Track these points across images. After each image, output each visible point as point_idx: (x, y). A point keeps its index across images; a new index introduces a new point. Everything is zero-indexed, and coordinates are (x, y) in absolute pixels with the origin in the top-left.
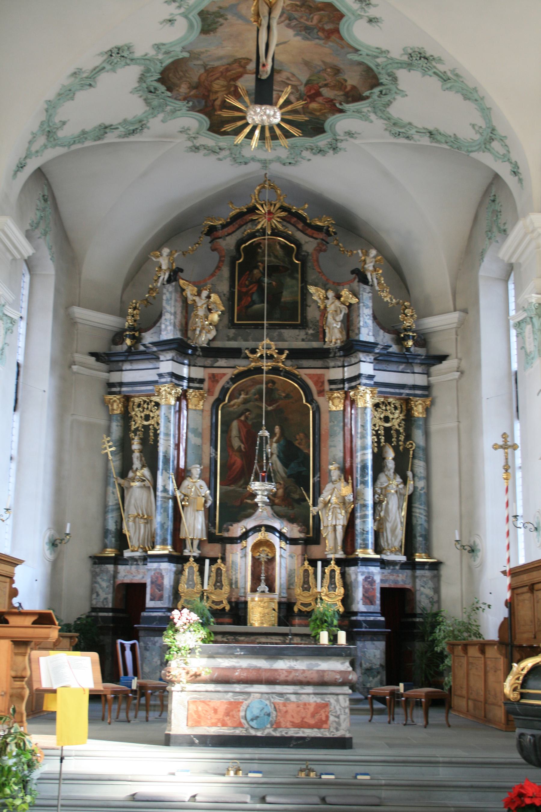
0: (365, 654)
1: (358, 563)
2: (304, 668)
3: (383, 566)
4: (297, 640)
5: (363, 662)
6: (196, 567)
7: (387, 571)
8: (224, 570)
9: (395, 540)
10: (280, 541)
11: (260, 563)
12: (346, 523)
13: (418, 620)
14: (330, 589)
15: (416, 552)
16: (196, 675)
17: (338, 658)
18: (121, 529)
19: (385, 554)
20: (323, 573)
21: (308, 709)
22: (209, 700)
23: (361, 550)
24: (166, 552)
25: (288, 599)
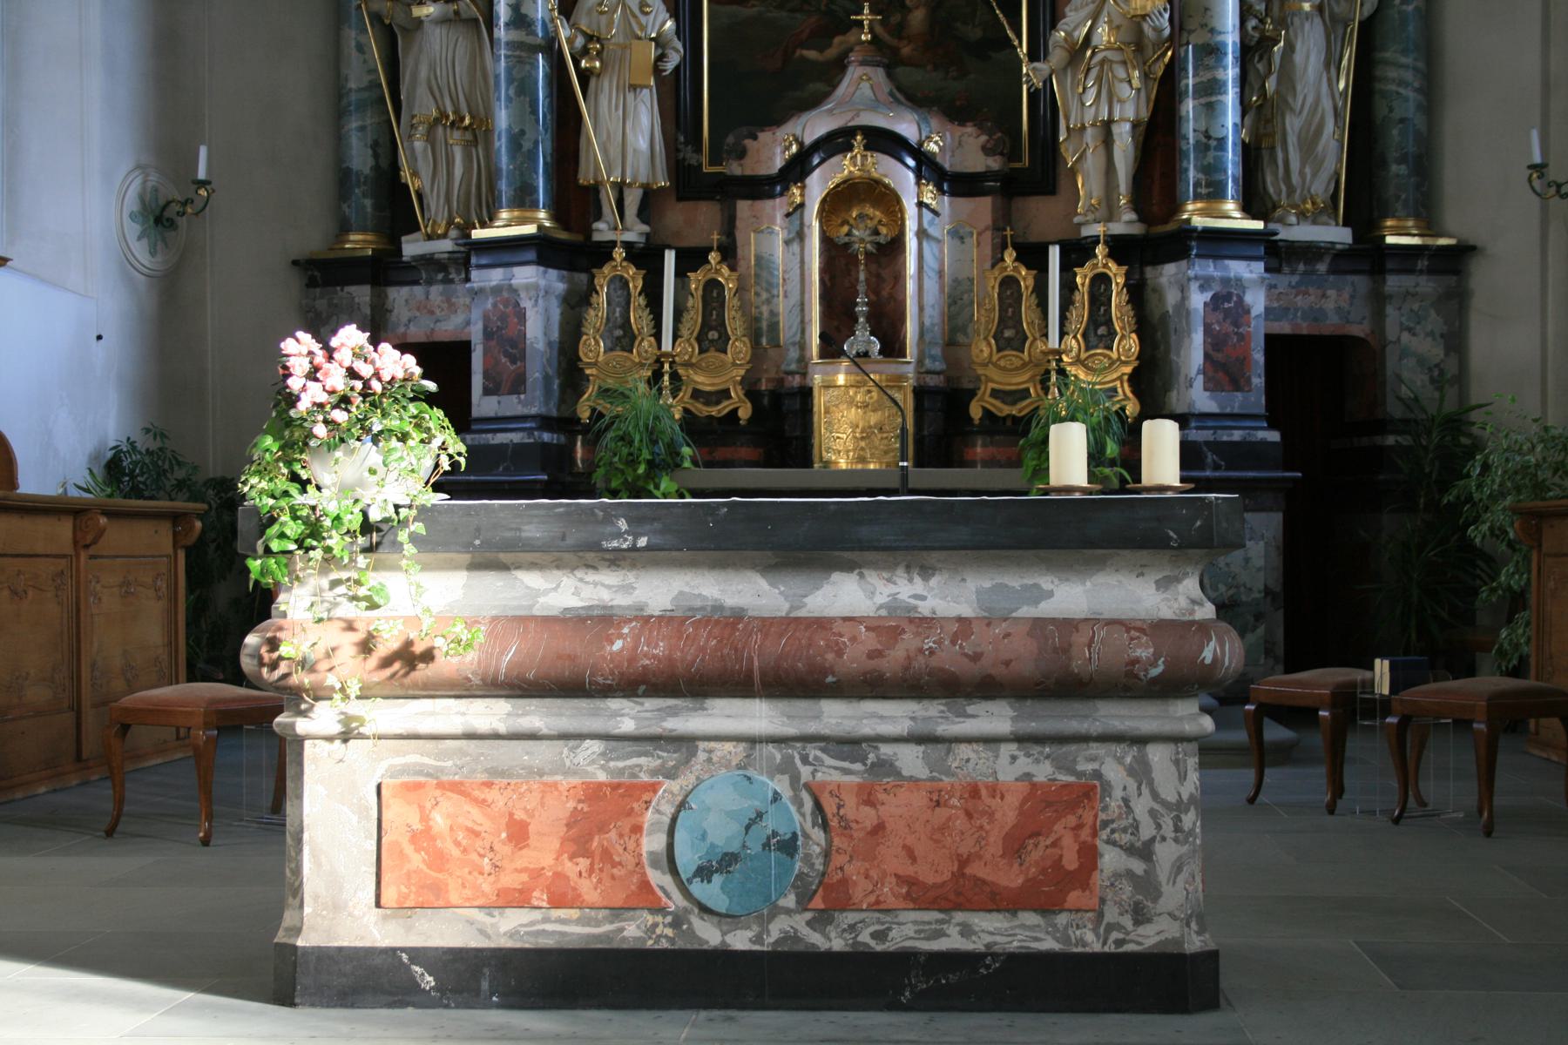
1: (1189, 249)
2: (967, 611)
3: (1274, 263)
6: (635, 279)
7: (1284, 281)
9: (1314, 175)
10: (918, 183)
11: (854, 259)
12: (1145, 115)
13: (1391, 440)
14: (1093, 339)
15: (1386, 216)
16: (409, 657)
17: (1144, 555)
18: (395, 167)
19: (1281, 220)
20: (1068, 287)
22: (483, 777)
23: (1199, 205)
24: (530, 229)
25: (948, 379)
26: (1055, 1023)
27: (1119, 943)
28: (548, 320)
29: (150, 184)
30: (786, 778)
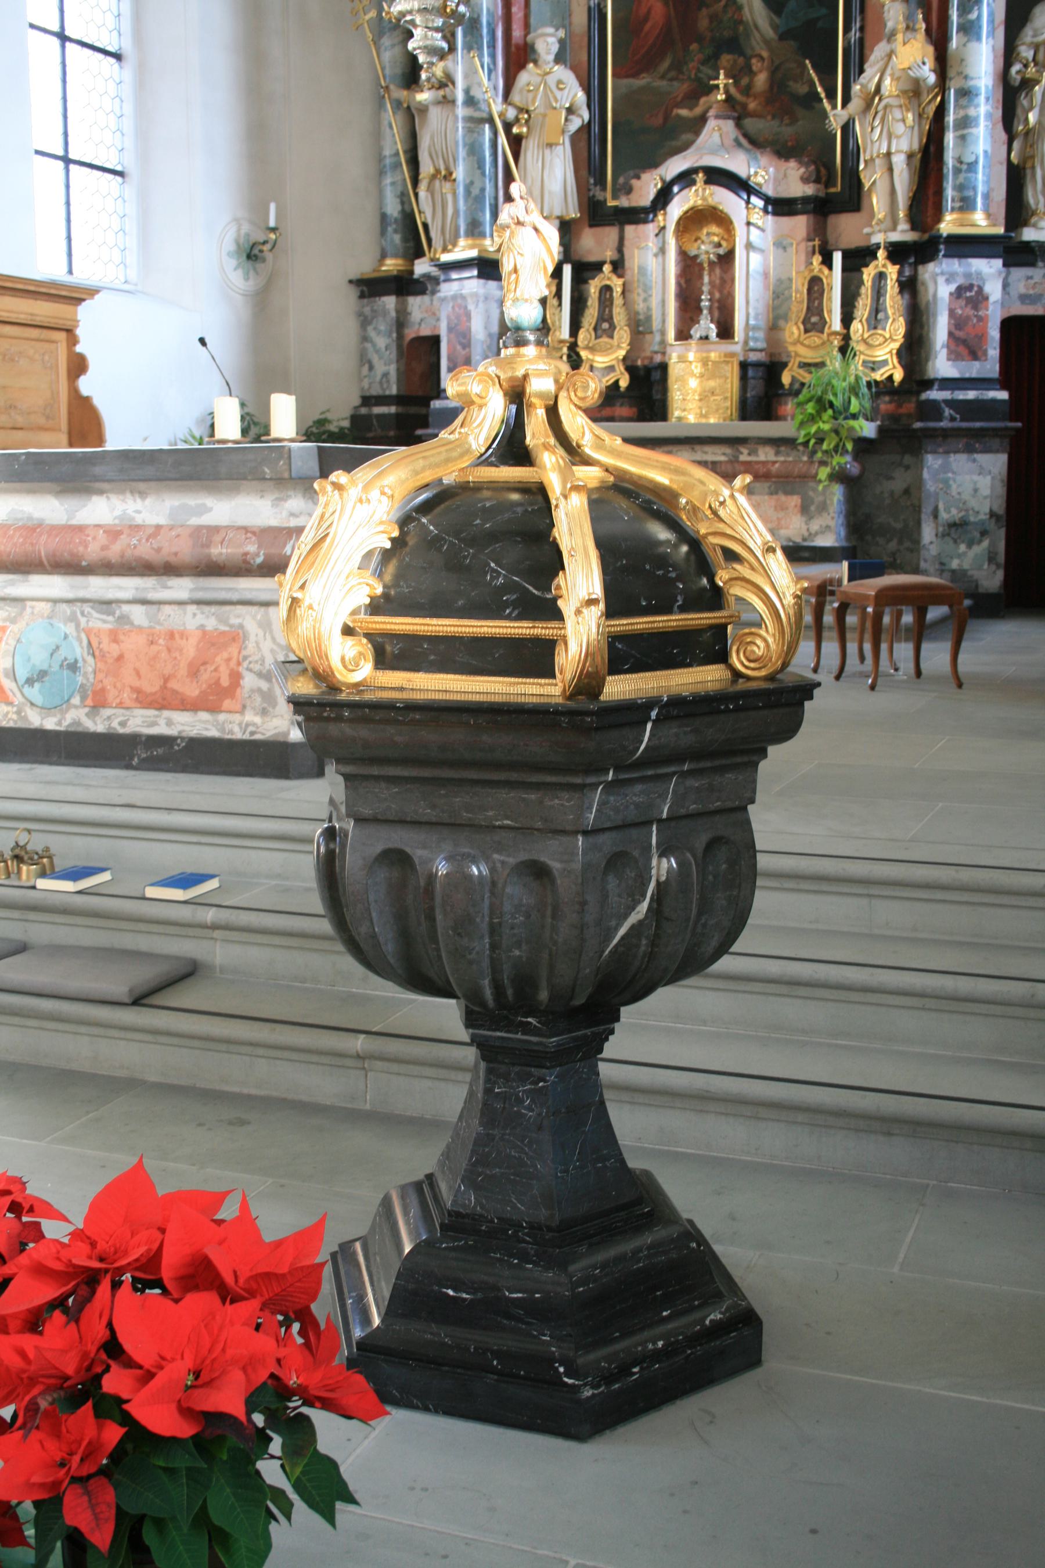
0: (949, 487)
2: (162, 521)
4: (766, 454)
5: (941, 506)
8: (618, 290)
11: (701, 265)
21: (181, 650)
25: (771, 355)
26: (168, 781)
27: (252, 733)
28: (488, 317)
29: (243, 232)
30: (73, 625)
